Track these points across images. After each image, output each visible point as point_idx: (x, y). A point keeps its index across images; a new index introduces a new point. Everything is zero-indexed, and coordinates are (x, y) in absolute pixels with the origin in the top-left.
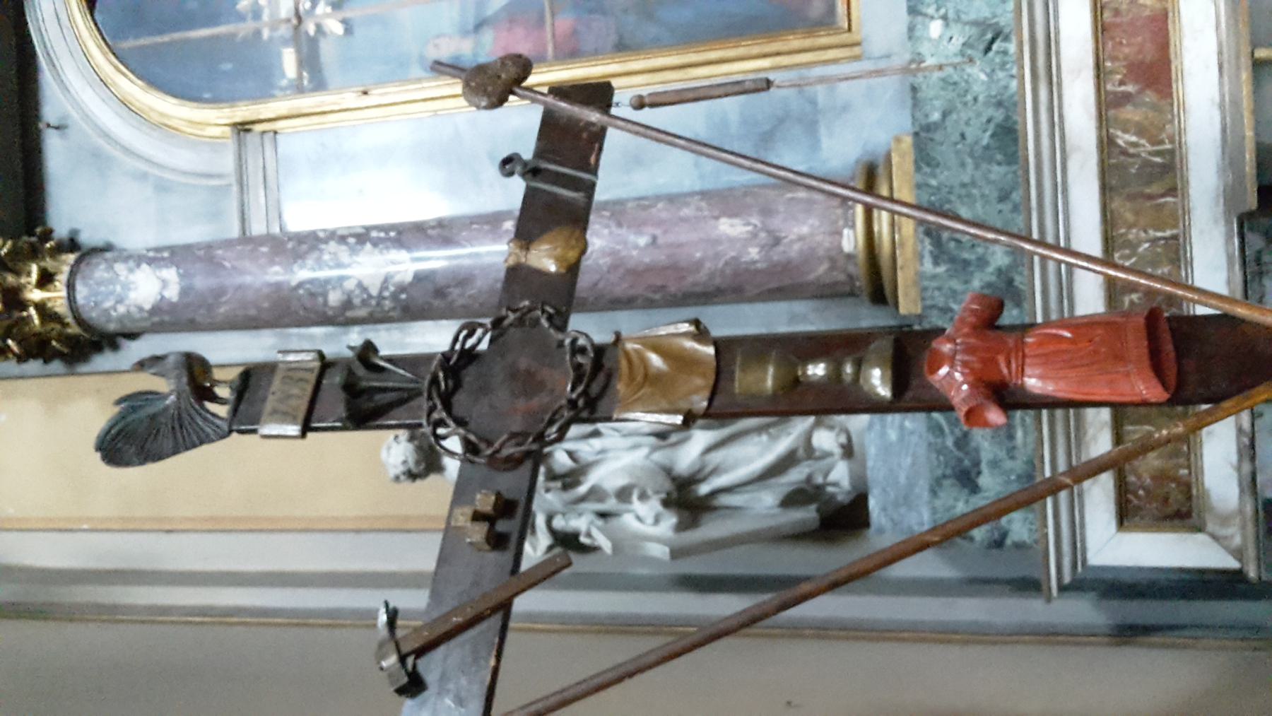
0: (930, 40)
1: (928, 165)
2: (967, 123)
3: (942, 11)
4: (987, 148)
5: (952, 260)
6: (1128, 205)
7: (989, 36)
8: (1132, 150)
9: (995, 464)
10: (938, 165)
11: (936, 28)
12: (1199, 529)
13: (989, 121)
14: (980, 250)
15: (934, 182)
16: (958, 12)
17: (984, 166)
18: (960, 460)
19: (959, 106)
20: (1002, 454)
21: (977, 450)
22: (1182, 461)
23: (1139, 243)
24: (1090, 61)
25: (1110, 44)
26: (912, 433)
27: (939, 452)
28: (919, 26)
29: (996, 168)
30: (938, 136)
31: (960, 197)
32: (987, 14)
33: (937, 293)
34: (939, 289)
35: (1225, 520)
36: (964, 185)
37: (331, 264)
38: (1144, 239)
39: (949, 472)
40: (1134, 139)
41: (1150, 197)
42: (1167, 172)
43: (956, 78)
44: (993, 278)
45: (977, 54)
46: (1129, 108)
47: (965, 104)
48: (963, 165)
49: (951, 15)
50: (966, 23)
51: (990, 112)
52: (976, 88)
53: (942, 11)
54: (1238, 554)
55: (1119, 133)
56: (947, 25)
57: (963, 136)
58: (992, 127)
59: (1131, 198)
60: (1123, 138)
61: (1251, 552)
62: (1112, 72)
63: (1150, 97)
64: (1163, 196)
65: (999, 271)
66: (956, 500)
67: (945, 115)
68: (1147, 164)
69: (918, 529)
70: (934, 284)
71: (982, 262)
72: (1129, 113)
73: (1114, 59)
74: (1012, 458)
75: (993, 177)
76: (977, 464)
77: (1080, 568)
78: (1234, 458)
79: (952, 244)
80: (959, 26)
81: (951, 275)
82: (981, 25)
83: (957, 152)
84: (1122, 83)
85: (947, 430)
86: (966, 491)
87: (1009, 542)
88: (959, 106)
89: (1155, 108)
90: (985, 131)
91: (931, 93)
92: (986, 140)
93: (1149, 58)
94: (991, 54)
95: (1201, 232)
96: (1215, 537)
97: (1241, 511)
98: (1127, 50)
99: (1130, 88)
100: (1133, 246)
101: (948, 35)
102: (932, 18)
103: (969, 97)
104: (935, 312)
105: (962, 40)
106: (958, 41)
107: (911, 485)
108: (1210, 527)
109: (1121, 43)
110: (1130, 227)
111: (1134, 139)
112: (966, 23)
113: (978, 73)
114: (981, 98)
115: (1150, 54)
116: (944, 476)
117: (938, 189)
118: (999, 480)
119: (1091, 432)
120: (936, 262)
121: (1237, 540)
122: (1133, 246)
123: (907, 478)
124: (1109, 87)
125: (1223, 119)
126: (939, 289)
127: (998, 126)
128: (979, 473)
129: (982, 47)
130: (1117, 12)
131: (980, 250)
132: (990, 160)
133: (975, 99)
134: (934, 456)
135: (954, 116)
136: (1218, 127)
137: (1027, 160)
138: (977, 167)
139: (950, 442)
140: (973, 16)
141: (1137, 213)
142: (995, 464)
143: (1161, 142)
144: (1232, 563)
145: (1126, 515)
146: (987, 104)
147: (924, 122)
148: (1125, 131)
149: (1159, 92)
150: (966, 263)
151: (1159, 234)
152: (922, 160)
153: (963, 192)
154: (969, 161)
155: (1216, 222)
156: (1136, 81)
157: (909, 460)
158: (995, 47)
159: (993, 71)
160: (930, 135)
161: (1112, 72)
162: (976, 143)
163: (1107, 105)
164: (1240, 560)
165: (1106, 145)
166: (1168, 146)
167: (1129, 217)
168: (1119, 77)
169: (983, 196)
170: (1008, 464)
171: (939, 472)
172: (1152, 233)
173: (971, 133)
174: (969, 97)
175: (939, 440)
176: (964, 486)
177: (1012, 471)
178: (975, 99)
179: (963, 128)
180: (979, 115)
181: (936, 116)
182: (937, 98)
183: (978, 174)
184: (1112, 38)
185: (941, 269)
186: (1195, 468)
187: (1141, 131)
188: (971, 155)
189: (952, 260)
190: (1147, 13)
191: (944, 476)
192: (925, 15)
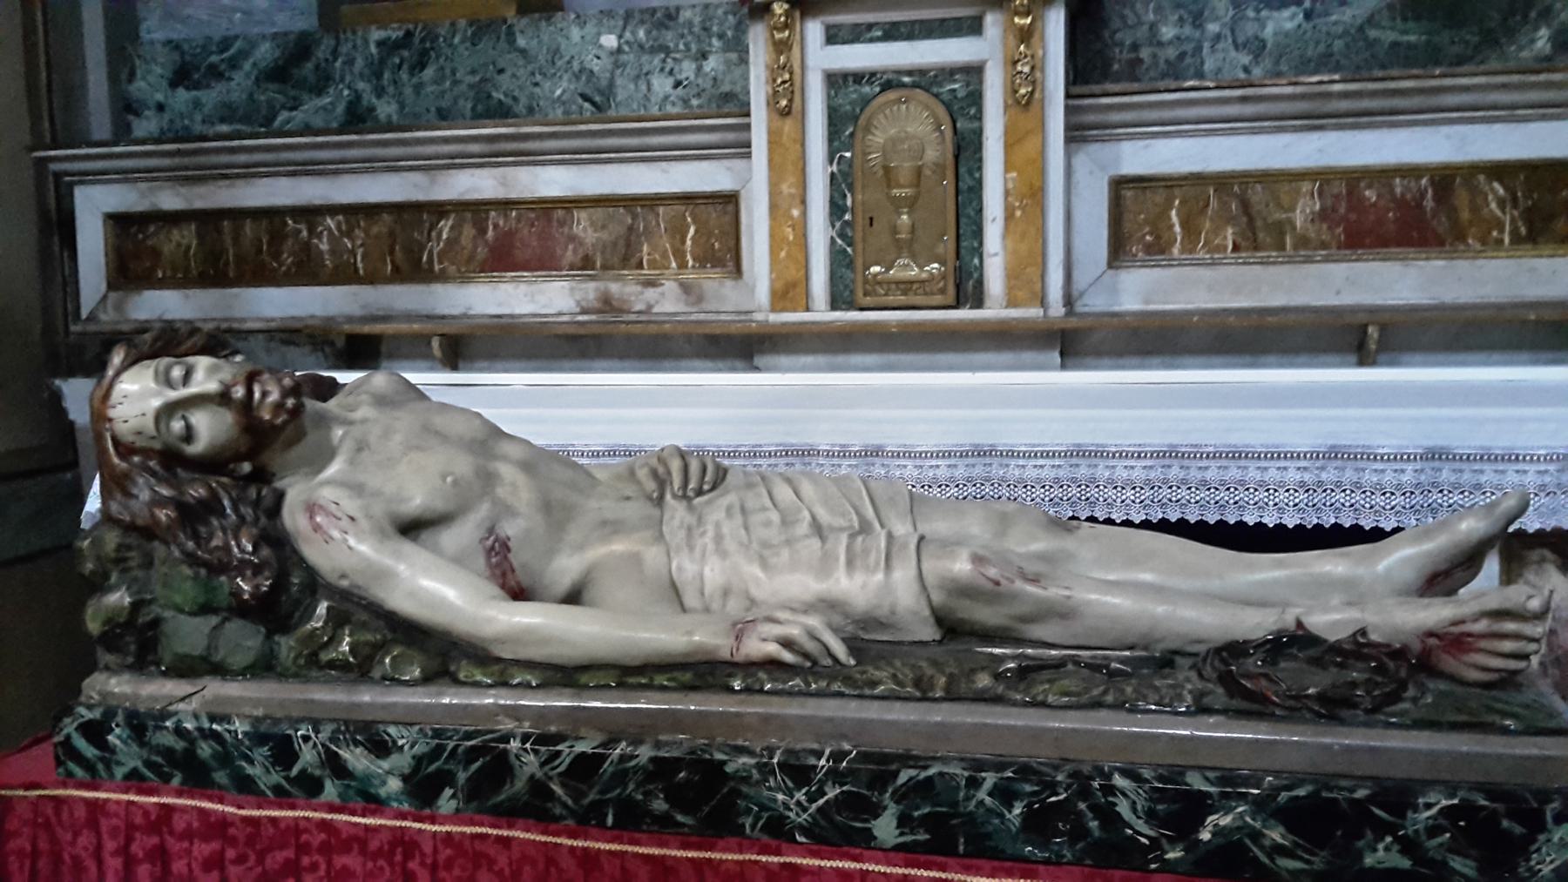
0: (599, 34)
1: (474, 34)
2: (514, 75)
3: (626, 48)
4: (489, 96)
5: (382, 61)
6: (385, 230)
7: (597, 99)
8: (434, 234)
9: (197, 104)
10: (474, 45)
11: (610, 41)
12: (112, 286)
13: (515, 99)
14: (391, 90)
15: (456, 40)
16: (624, 65)
17: (472, 94)
18: (198, 69)
19: (530, 68)
20: (206, 110)
21: (208, 86)
22: (169, 273)
23: (352, 240)
24: (513, 195)
25: (533, 215)
26: (231, 21)
27: (204, 47)
28: (612, 23)
29: (469, 106)
30: (503, 44)
31: (442, 68)
32: (619, 98)
33: (350, 45)
34: (354, 47)
35: (119, 307)
36: (454, 72)
37: (1469, 52)
38: (356, 245)
39: (188, 58)
40: (445, 236)
41: (392, 252)
42: (416, 271)
43: (559, 63)
44: (365, 103)
45: (581, 86)
46: (473, 232)
47: (533, 74)
48: (473, 72)
49: (624, 58)
50: (612, 74)
51: (523, 101)
52: (547, 85)
53: (626, 48)
54: (92, 317)
55: (450, 223)
56: (612, 53)
57: (501, 71)
58: (509, 101)
59: (392, 234)
60: (445, 226)
61: (92, 328)
62: (506, 216)
63: (482, 252)
64: (393, 262)
65: (372, 109)
66: (163, 65)
67: (523, 52)
68: (422, 248)
69: (144, 27)
70: (359, 42)
71: (380, 92)
72: (468, 231)
73: (518, 219)
74: (204, 122)
75: (461, 102)
76: (197, 86)
77: (68, 178)
78: (169, 316)
79: (397, 61)
80: (610, 67)
81: (370, 63)
82: (609, 91)
83: (486, 65)
84: (496, 226)
85: (225, 55)
86: (169, 74)
87: (131, 117)
88: (530, 68)
89: (471, 259)
90: (506, 95)
91: (545, 38)
92: (497, 95)
93: (517, 252)
94: (580, 101)
95: (355, 294)
96: (105, 297)
97: (128, 321)
98: (526, 231)
99: (490, 233)
100: (349, 234)
101: (602, 55)
102: (620, 37)
103: (538, 78)
104: (333, 42)
105: (596, 69)
106: (596, 65)
107: (185, 20)
108: (113, 295)
109: (532, 225)
110: (367, 232)
111: (445, 236)
112: (612, 74)
113: (561, 88)
114: (537, 90)
115: (520, 254)
116: (183, 54)
117: (450, 45)
118: (184, 109)
119: (183, 190)
120: (380, 44)
121: (103, 317)
122: (349, 234)
123: (189, 16)
124: (493, 213)
125: (454, 317)
126: (354, 47)
127: (510, 108)
128: (187, 88)
129: (588, 91)
130: (562, 223)
131: (391, 90)
132: (477, 100)
133: (536, 84)
134: (201, 42)
135: (521, 62)
136: (446, 311)
137: (439, 129)
138: (471, 86)
139: (214, 59)
140: (619, 81)
141: (377, 237)
142: (197, 104)
143: (440, 262)
144: (84, 314)
145: (120, 223)
146: (532, 96)
147: (516, 29)
148: (452, 228)
149: (485, 261)
150: (378, 75)
151: (359, 258)
152: (480, 28)
153: (448, 71)
154: (477, 78)
155: (364, 307)
156: (496, 239)
157: (205, 17)
158: (587, 105)
159: (564, 103)
160: (503, 36)
161: (506, 216)
162: (494, 85)
163: (476, 210)
164: (88, 319)
165: (439, 209)
166: (437, 267)
167: (375, 230)
168: (501, 223)
169: (443, 92)
170: (198, 118)
171: (186, 47)
172: (360, 252)
173: (504, 80)
174: (538, 78)
175: (214, 48)
176: (176, 73)
177: (192, 120)
178: (536, 84)
179: (509, 73)
180: (521, 88)
181: (521, 42)
182: (540, 42)
183: (463, 87)
184: (537, 219)
185: (373, 49)
186: (162, 284)
187: (451, 242)
188: (484, 80)
189: (382, 61)
190: (559, 252)
191: (183, 54)
192: (624, 28)
